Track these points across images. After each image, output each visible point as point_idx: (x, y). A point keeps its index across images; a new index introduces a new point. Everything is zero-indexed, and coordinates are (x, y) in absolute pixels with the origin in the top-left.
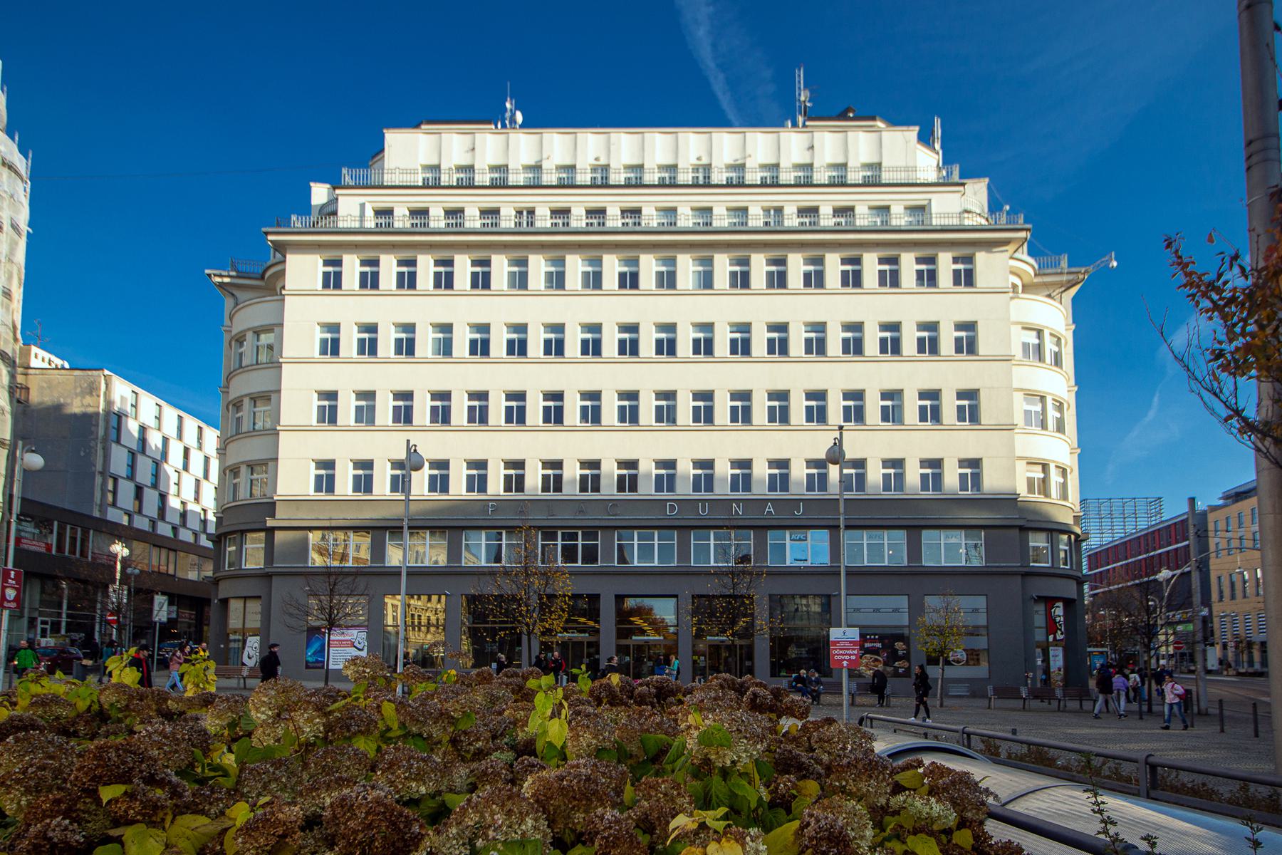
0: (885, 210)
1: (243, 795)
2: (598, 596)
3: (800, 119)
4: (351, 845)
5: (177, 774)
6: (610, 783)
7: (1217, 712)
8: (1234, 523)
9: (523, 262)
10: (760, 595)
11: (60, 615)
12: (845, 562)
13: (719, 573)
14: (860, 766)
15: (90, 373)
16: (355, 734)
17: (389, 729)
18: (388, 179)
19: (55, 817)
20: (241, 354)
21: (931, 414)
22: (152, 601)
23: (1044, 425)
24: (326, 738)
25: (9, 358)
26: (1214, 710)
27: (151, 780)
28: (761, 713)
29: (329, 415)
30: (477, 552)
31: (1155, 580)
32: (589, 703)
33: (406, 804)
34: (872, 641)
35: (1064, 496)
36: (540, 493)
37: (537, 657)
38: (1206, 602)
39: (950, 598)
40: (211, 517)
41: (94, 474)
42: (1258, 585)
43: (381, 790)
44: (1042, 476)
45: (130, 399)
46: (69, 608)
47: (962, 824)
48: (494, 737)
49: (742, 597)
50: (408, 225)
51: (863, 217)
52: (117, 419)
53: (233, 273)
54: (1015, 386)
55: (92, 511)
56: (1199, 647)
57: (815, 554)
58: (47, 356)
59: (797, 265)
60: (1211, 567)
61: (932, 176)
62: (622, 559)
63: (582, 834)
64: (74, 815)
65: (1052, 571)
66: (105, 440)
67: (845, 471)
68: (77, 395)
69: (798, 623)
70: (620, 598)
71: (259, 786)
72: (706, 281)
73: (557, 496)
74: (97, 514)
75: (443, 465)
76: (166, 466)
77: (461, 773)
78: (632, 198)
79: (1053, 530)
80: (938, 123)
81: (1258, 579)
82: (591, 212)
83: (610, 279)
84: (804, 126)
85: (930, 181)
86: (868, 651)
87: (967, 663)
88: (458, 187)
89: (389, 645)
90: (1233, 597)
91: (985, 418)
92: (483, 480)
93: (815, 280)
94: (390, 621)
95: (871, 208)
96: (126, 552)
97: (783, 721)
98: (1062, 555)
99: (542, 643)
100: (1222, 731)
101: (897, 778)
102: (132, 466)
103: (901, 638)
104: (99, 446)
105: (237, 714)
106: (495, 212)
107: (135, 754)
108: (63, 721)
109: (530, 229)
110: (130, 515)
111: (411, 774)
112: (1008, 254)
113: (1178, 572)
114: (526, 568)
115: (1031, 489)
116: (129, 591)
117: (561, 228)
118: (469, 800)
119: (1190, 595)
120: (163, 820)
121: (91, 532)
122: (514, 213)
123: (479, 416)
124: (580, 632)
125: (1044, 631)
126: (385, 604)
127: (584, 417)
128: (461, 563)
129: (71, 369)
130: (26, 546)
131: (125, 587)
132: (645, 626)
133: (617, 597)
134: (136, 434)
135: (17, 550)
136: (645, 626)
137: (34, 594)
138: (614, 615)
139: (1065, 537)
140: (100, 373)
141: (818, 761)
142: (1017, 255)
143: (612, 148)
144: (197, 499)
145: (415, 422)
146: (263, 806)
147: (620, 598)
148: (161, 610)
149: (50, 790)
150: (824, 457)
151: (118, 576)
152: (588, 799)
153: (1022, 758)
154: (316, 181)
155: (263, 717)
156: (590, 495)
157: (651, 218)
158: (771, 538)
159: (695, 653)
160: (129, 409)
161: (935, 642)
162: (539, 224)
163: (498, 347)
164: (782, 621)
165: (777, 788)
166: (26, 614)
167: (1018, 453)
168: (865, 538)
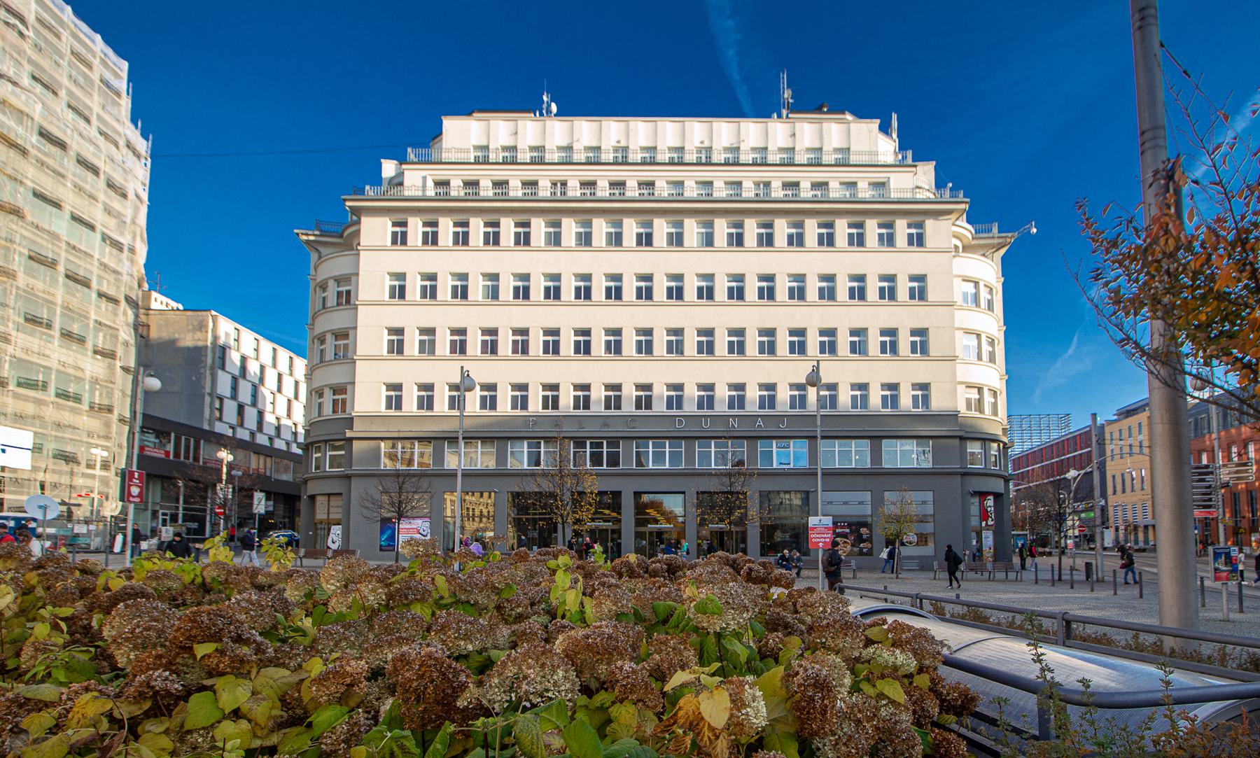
0: (852, 185)
1: (318, 651)
2: (620, 493)
3: (784, 112)
4: (407, 691)
5: (261, 634)
6: (628, 641)
7: (1112, 579)
8: (1125, 434)
9: (557, 224)
10: (753, 490)
11: (177, 508)
12: (821, 465)
13: (719, 474)
14: (837, 626)
15: (199, 313)
16: (411, 602)
17: (442, 598)
18: (445, 157)
19: (158, 669)
20: (324, 299)
21: (890, 347)
22: (252, 497)
23: (980, 358)
24: (387, 605)
25: (134, 302)
26: (1109, 578)
27: (239, 639)
28: (754, 583)
29: (397, 347)
30: (520, 457)
31: (1065, 478)
32: (613, 577)
33: (457, 659)
34: (842, 527)
35: (995, 413)
36: (572, 410)
37: (569, 542)
38: (1104, 494)
39: (904, 493)
40: (301, 430)
41: (203, 396)
42: (1143, 482)
43: (436, 648)
44: (977, 397)
45: (233, 335)
46: (185, 502)
47: (921, 670)
48: (532, 604)
49: (738, 493)
50: (462, 194)
51: (835, 191)
52: (222, 352)
53: (318, 233)
54: (957, 325)
55: (202, 424)
56: (1098, 530)
57: (797, 458)
58: (165, 300)
59: (782, 229)
60: (1107, 468)
61: (890, 159)
62: (639, 463)
63: (604, 683)
64: (174, 668)
65: (985, 471)
66: (212, 368)
67: (822, 393)
68: (189, 331)
69: (783, 514)
70: (638, 495)
71: (332, 643)
72: (709, 240)
73: (586, 413)
74: (206, 427)
75: (492, 387)
76: (262, 389)
77: (504, 632)
78: (647, 174)
79: (986, 440)
80: (894, 116)
81: (1142, 478)
82: (613, 184)
83: (629, 239)
84: (787, 117)
85: (889, 163)
86: (838, 535)
87: (917, 544)
88: (503, 163)
89: (449, 533)
90: (1124, 491)
91: (933, 351)
92: (525, 400)
93: (797, 240)
94: (449, 513)
95: (841, 183)
96: (231, 458)
97: (773, 590)
98: (993, 459)
99: (574, 531)
100: (1115, 594)
101: (867, 633)
102: (235, 388)
103: (865, 525)
104: (208, 372)
105: (313, 586)
106: (534, 184)
107: (224, 617)
108: (174, 592)
109: (563, 198)
110: (232, 427)
111: (459, 634)
112: (951, 222)
113: (1082, 472)
114: (561, 471)
115: (969, 407)
116: (234, 488)
117: (588, 197)
118: (509, 656)
119: (1092, 489)
120: (249, 672)
121: (202, 441)
122: (550, 185)
123: (521, 348)
124: (605, 521)
125: (978, 518)
126: (445, 500)
127: (608, 350)
128: (379, 465)
129: (185, 310)
130: (149, 453)
131: (231, 486)
132: (658, 517)
133: (635, 493)
134: (238, 363)
135: (139, 456)
136: (658, 517)
137: (155, 494)
138: (633, 507)
139: (995, 445)
140: (208, 313)
141: (803, 622)
142: (958, 223)
143: (631, 133)
144: (289, 415)
145: (562, 353)
146: (334, 661)
147: (638, 495)
148: (260, 504)
149: (155, 646)
150: (804, 381)
151: (224, 477)
152: (610, 654)
153: (963, 617)
154: (385, 158)
155: (333, 588)
156: (613, 412)
157: (663, 189)
158: (760, 446)
159: (699, 538)
160: (232, 343)
161: (892, 528)
162: (570, 194)
163: (537, 293)
164: (769, 513)
165: (767, 643)
166: (150, 508)
167: (959, 379)
168: (837, 446)
